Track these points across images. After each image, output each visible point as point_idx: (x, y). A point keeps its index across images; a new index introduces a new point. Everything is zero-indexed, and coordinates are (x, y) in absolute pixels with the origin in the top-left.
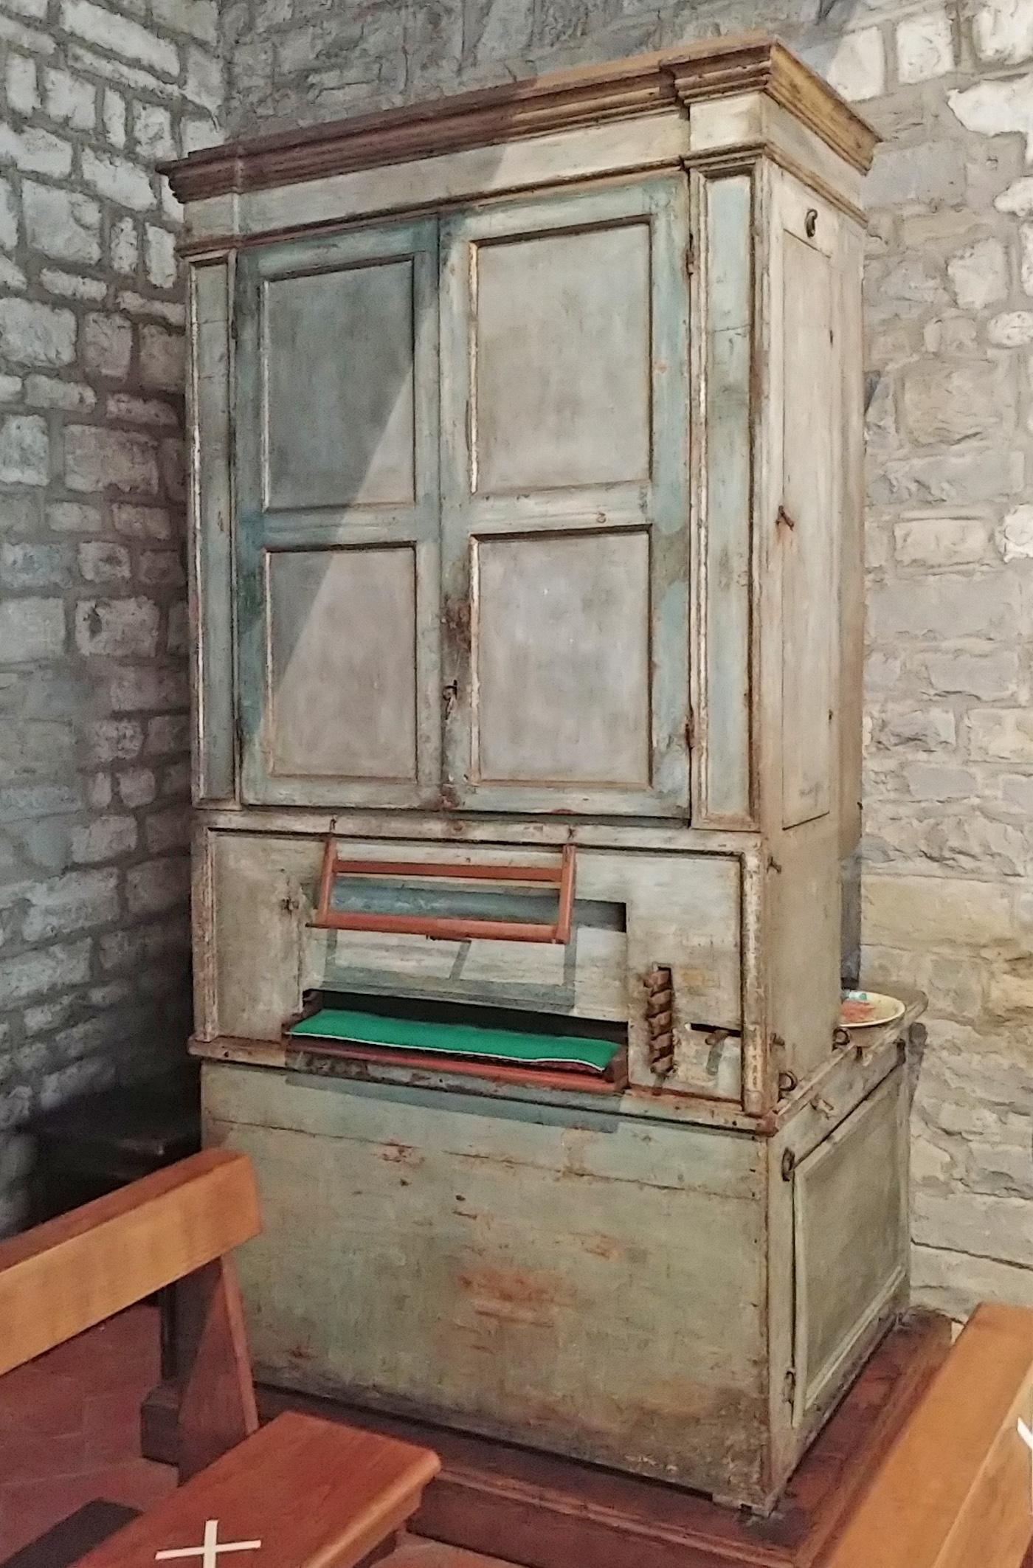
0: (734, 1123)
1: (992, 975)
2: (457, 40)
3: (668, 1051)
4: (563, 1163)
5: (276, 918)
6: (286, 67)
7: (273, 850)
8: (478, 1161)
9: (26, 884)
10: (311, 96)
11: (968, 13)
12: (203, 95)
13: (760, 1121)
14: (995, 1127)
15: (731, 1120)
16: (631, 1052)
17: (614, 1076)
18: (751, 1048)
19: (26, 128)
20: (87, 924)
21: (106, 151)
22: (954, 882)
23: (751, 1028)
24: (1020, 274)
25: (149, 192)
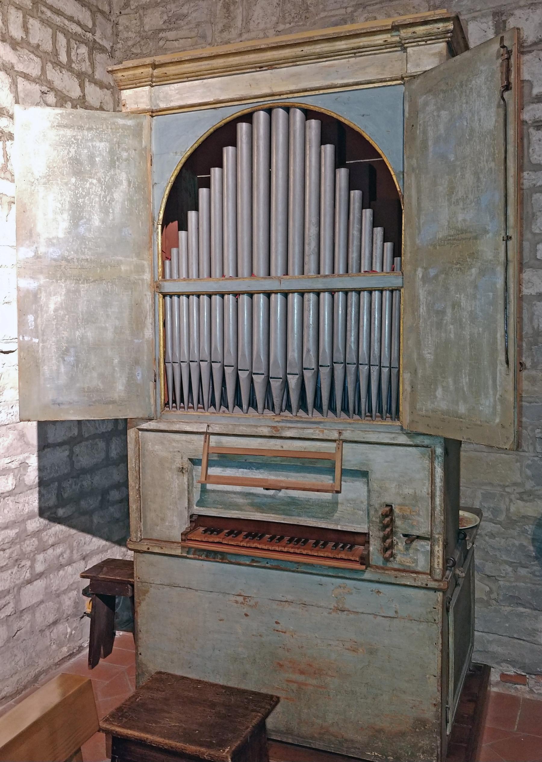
0: (427, 585)
1: (511, 500)
2: (240, 18)
3: (391, 546)
4: (333, 605)
5: (175, 477)
6: (147, 28)
7: (174, 440)
8: (287, 603)
9: (26, 455)
10: (161, 43)
11: (504, 18)
12: (104, 40)
13: (440, 583)
14: (511, 574)
15: (425, 583)
16: (371, 549)
17: (364, 560)
18: (437, 546)
19: (18, 48)
20: (56, 475)
21: (57, 64)
22: (492, 454)
23: (437, 536)
24: (528, 153)
25: (78, 89)
